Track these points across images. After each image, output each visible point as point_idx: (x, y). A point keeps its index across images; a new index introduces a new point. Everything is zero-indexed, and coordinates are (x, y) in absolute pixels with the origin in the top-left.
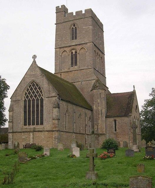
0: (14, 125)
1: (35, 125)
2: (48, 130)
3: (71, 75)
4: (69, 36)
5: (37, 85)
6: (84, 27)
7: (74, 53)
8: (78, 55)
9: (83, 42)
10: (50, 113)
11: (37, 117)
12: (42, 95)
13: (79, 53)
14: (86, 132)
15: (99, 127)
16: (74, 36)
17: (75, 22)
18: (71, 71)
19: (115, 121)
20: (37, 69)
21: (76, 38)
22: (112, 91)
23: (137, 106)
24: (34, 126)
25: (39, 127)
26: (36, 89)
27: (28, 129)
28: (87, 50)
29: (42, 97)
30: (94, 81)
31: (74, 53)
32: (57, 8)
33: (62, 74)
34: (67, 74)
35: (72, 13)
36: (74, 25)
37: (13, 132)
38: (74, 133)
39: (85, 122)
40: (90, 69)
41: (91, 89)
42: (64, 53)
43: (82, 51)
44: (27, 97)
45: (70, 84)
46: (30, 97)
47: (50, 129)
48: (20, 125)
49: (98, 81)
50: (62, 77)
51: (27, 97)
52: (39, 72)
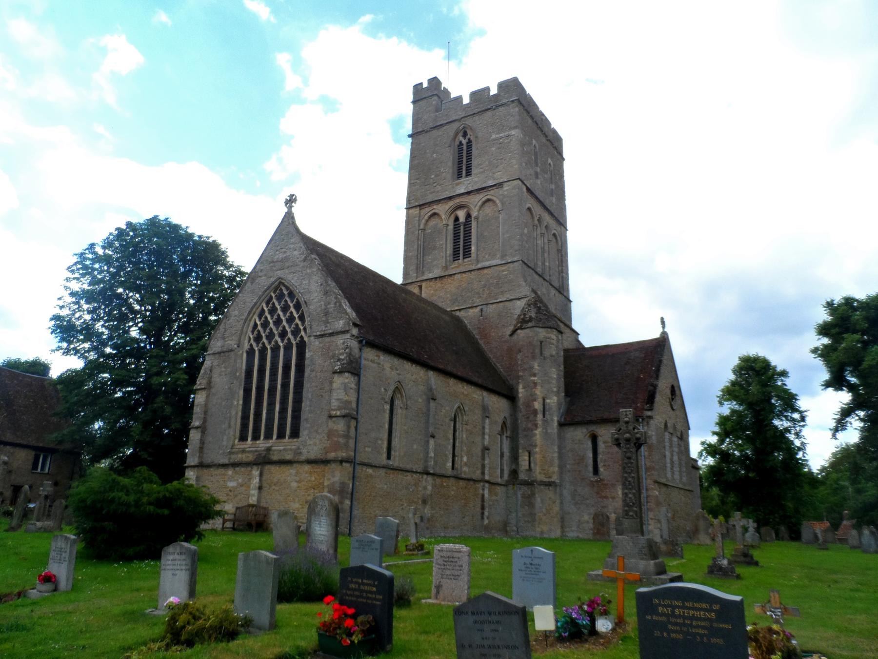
0: (209, 439)
1: (275, 437)
2: (312, 456)
3: (451, 286)
4: (448, 167)
5: (291, 295)
6: (494, 136)
7: (462, 219)
8: (474, 224)
9: (491, 183)
10: (328, 392)
11: (283, 410)
12: (305, 329)
13: (477, 218)
14: (483, 473)
15: (538, 457)
16: (463, 164)
17: (469, 122)
18: (451, 275)
19: (594, 438)
20: (296, 239)
21: (469, 173)
22: (588, 341)
23: (676, 389)
24: (270, 443)
25: (282, 447)
26: (285, 309)
27: (249, 452)
28: (503, 204)
29: (302, 337)
30: (521, 304)
31: (462, 219)
32: (417, 88)
33: (424, 285)
34: (439, 284)
35: (459, 98)
36: (465, 135)
37: (201, 466)
38: (425, 477)
39: (483, 438)
40: (511, 265)
41: (511, 328)
42: (433, 222)
43: (488, 209)
44: (258, 339)
45: (450, 314)
46: (274, 335)
47: (319, 456)
48: (225, 438)
49: (537, 303)
50: (424, 295)
51: (258, 339)
52: (297, 252)
